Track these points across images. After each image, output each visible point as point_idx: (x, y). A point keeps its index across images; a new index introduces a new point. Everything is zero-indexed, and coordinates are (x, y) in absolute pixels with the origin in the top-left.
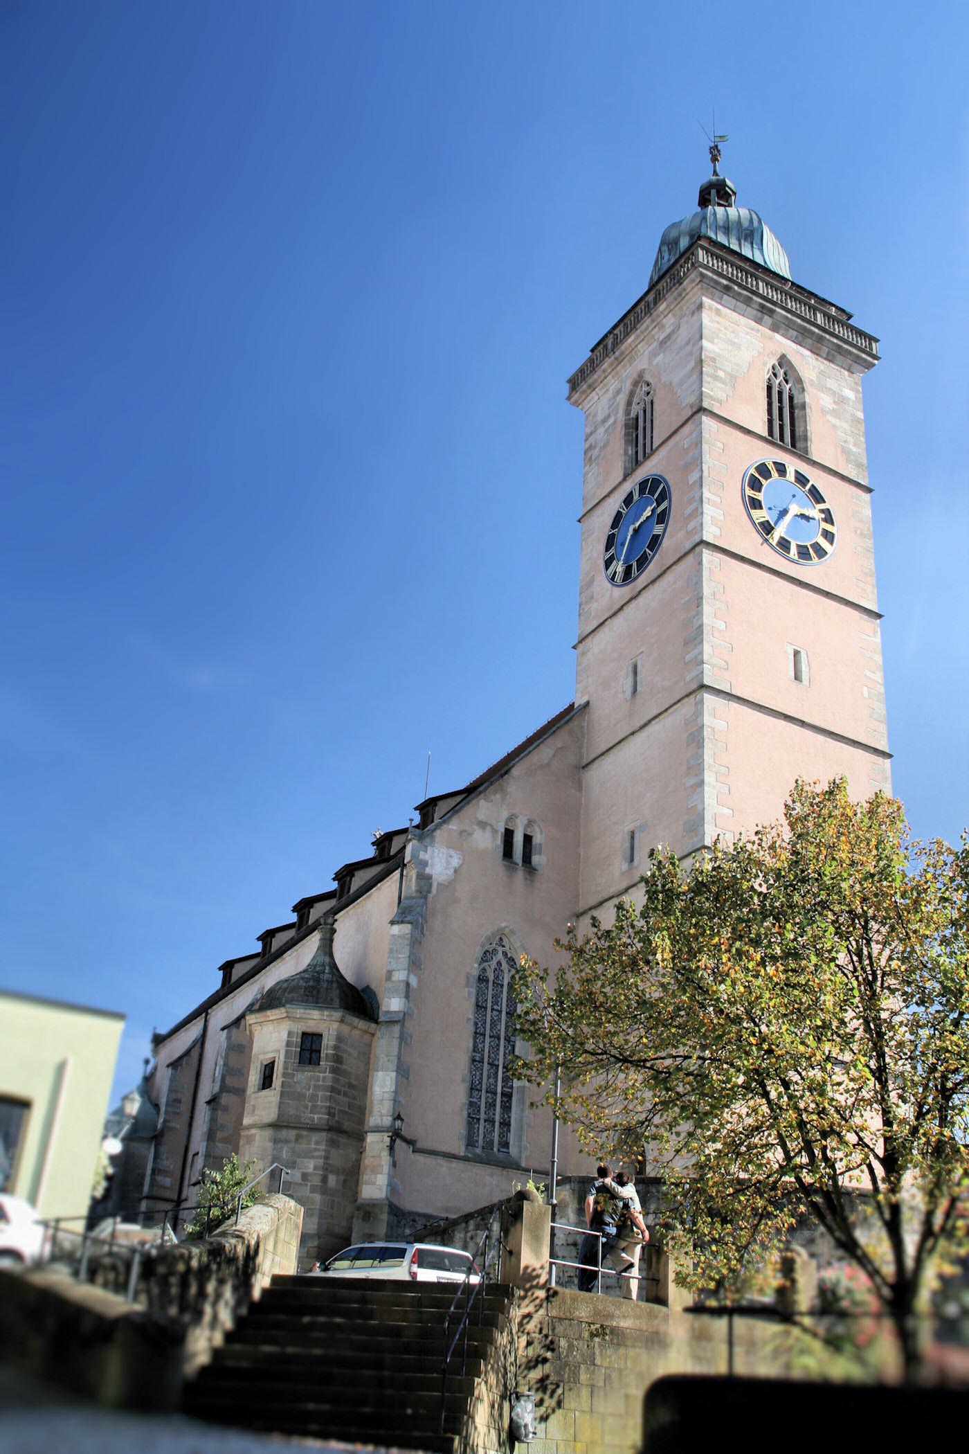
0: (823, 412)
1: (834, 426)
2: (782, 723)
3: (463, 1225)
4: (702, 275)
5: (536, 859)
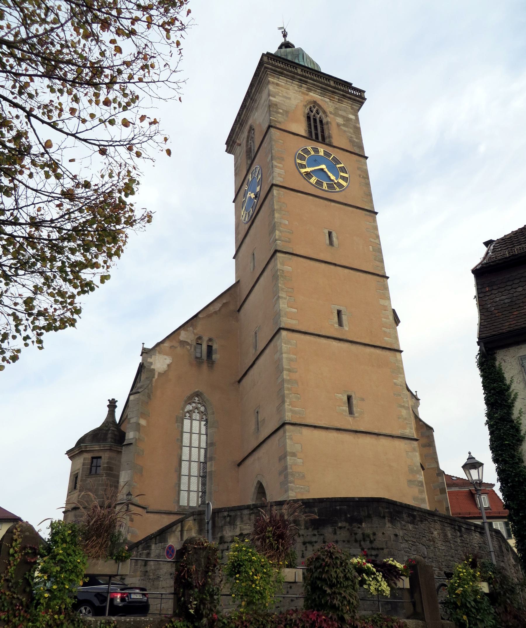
0: (338, 125)
1: (345, 131)
2: (323, 265)
3: (136, 549)
4: (266, 68)
5: (214, 356)
